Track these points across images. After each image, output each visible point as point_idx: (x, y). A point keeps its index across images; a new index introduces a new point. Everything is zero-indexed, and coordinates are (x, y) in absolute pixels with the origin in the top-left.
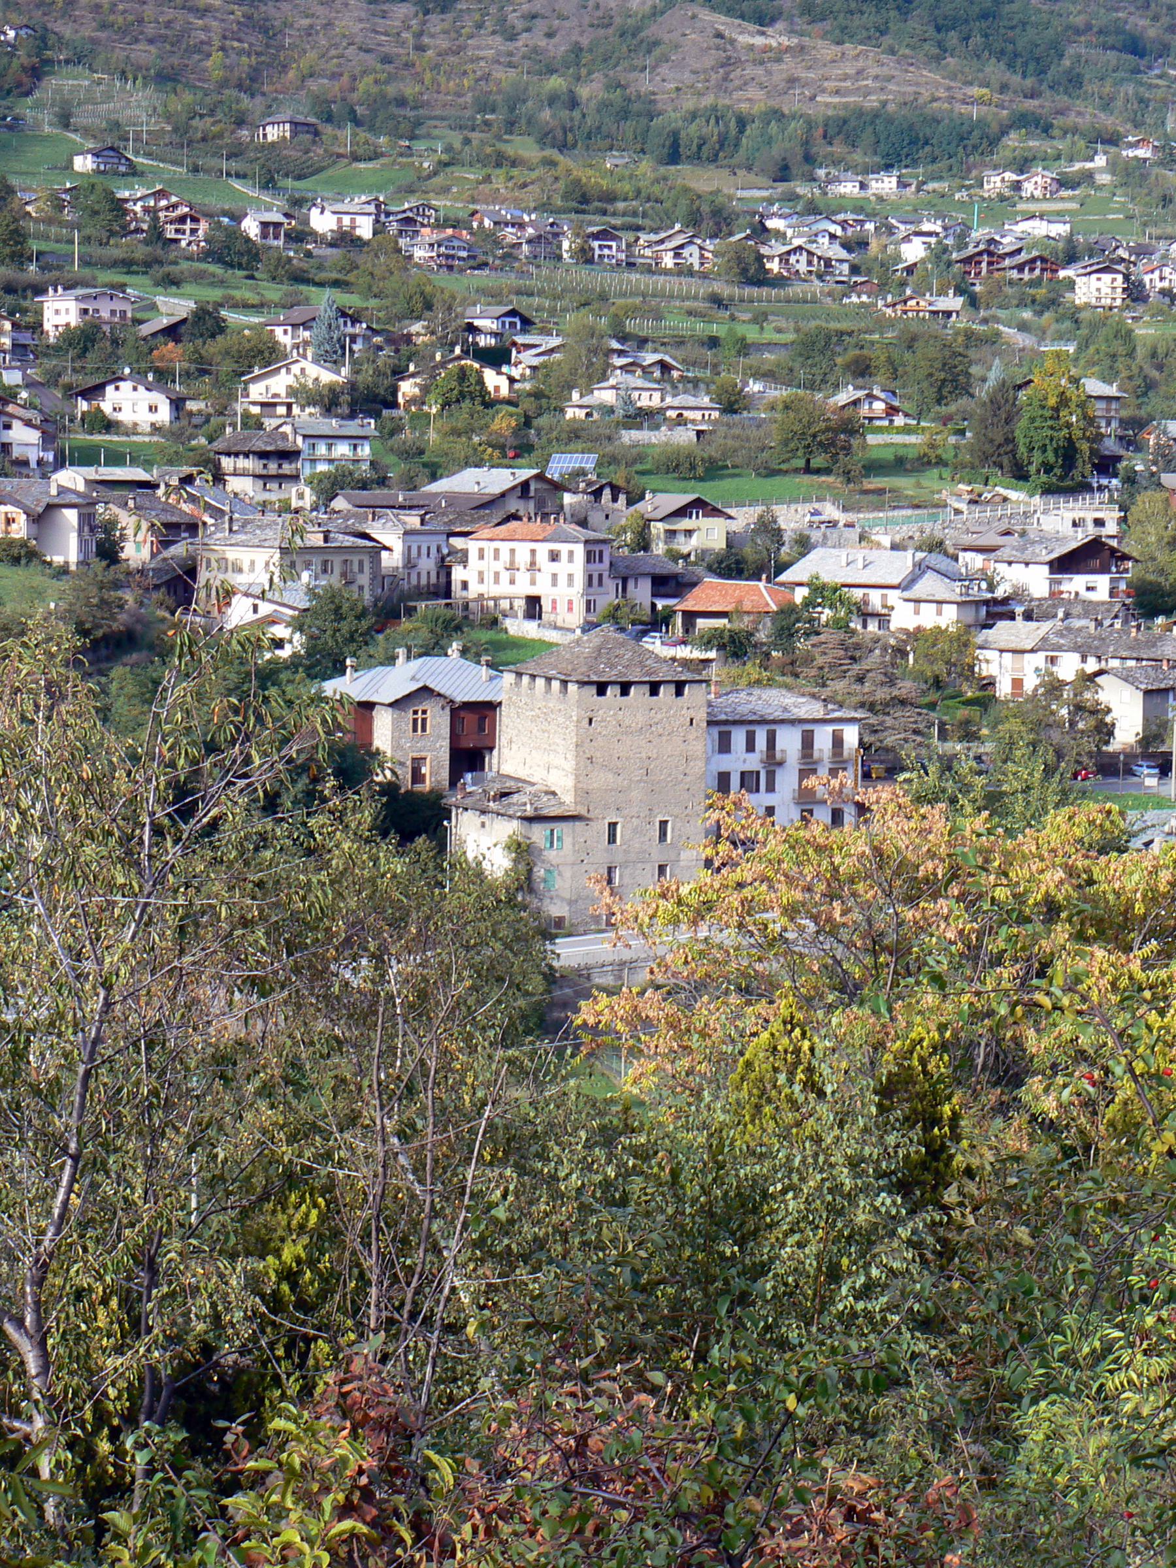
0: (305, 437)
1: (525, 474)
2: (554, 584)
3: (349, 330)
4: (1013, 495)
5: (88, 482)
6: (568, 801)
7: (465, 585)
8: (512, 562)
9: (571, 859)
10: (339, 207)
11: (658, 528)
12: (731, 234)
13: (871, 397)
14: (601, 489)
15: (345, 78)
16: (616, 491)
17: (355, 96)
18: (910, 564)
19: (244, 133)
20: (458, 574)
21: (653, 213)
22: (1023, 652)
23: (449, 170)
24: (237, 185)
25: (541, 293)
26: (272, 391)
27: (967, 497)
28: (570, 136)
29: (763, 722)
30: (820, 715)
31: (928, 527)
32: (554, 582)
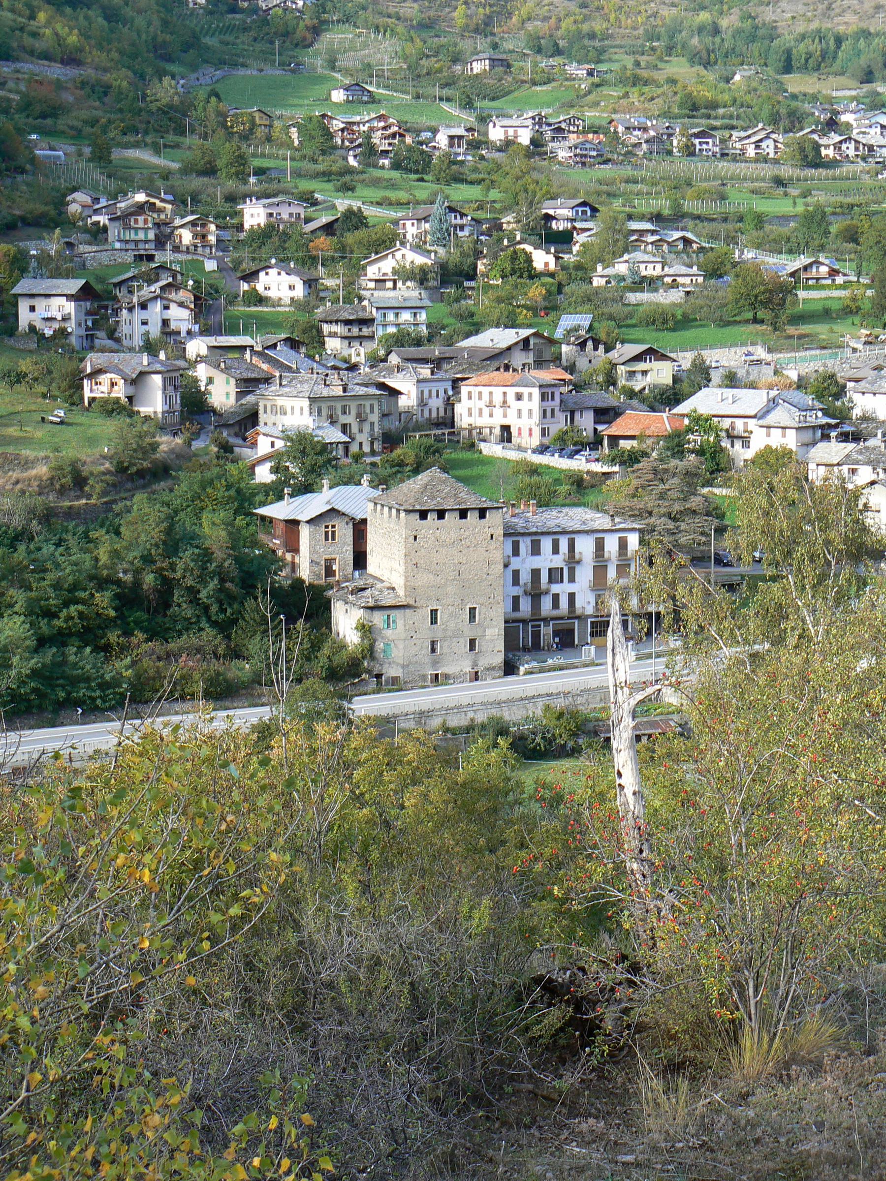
0: (378, 308)
1: (525, 333)
2: (520, 416)
3: (459, 221)
5: (211, 348)
8: (491, 401)
9: (403, 636)
10: (506, 122)
11: (622, 370)
12: (802, 129)
13: (818, 263)
14: (585, 341)
15: (553, 20)
16: (596, 343)
17: (559, 33)
18: (765, 400)
19: (458, 68)
21: (744, 116)
22: (834, 465)
23: (599, 89)
24: (445, 106)
25: (643, 180)
26: (383, 271)
27: (863, 339)
28: (712, 56)
29: (564, 532)
30: (608, 527)
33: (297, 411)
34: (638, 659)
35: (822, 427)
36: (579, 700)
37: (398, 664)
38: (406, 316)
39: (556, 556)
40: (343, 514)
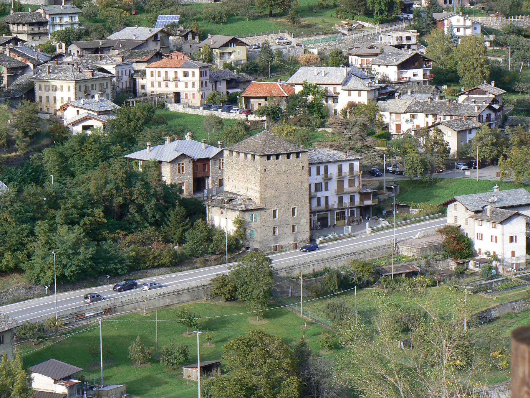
0: (49, 15)
4: (366, 24)
6: (257, 202)
7: (143, 87)
8: (166, 77)
11: (216, 52)
16: (194, 34)
18: (345, 74)
20: (139, 81)
30: (344, 158)
31: (333, 43)
32: (186, 86)
33: (65, 89)
34: (372, 232)
35: (378, 89)
36: (362, 256)
37: (257, 241)
38: (66, 19)
39: (319, 176)
40: (188, 157)
